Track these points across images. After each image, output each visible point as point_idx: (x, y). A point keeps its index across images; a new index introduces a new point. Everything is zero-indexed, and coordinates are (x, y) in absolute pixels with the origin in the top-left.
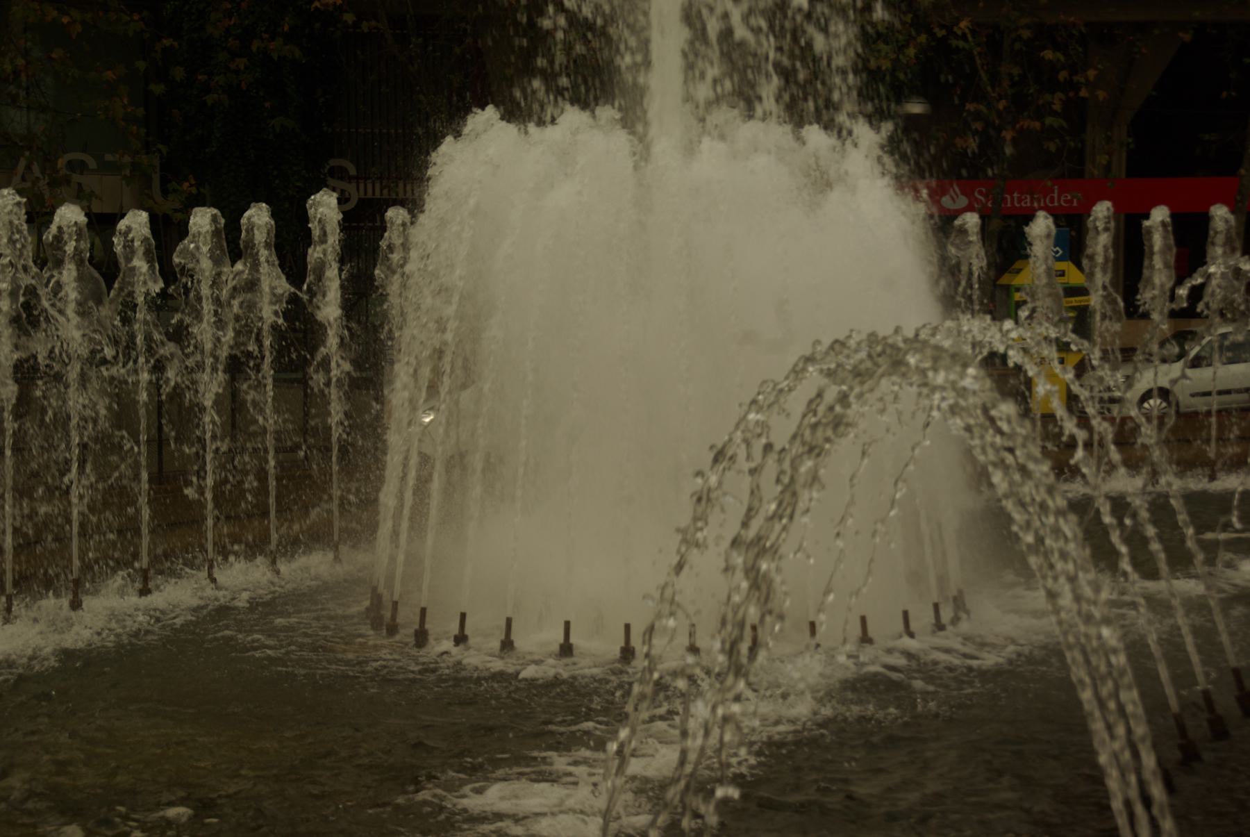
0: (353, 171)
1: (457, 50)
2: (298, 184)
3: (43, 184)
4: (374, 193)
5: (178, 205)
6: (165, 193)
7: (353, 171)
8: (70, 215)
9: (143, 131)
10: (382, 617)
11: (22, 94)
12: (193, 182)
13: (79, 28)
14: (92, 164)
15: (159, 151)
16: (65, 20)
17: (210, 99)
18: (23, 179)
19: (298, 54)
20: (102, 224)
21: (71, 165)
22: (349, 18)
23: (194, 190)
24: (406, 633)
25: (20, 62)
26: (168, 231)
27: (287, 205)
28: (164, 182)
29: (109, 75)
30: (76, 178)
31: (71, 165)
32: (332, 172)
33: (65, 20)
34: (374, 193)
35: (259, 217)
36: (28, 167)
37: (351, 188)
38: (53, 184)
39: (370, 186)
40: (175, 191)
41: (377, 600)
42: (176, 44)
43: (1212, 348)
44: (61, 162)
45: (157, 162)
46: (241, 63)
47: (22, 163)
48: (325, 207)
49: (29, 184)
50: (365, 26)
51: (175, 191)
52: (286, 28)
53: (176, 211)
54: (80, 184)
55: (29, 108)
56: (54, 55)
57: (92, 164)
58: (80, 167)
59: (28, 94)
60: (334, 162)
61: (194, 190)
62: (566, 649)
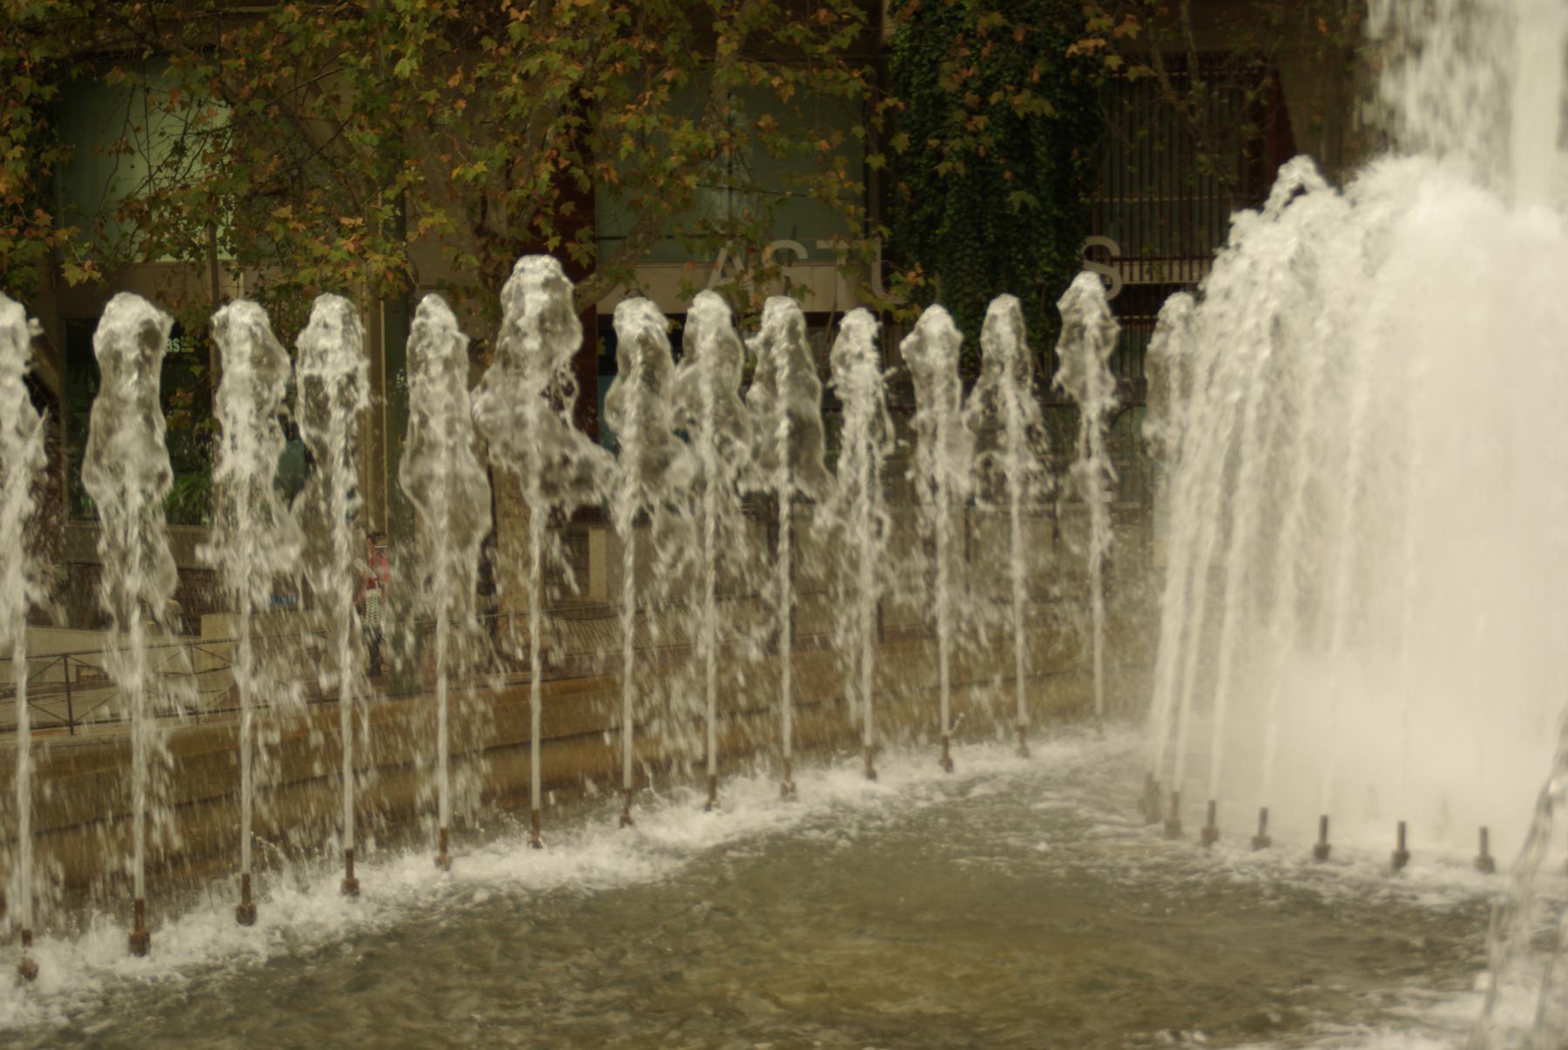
0: (1115, 251)
1: (1250, 95)
2: (1048, 269)
3: (748, 277)
4: (1131, 278)
5: (901, 301)
6: (887, 285)
7: (1115, 251)
8: (779, 312)
9: (862, 210)
10: (1157, 803)
11: (724, 172)
12: (920, 271)
13: (791, 91)
14: (802, 253)
15: (880, 234)
16: (776, 82)
17: (943, 168)
18: (724, 275)
19: (1048, 109)
20: (823, 325)
21: (777, 255)
22: (1113, 61)
23: (921, 281)
24: (1193, 828)
25: (724, 135)
26: (892, 330)
27: (1034, 296)
28: (886, 271)
29: (823, 145)
30: (786, 271)
31: (777, 255)
32: (1090, 254)
33: (776, 82)
34: (1131, 278)
35: (1003, 311)
36: (729, 260)
37: (1113, 272)
38: (760, 278)
39: (1176, 268)
40: (898, 283)
41: (1153, 788)
42: (901, 105)
43: (739, 629)
44: (768, 252)
45: (877, 247)
46: (981, 121)
47: (723, 253)
48: (1087, 294)
49: (731, 280)
50: (1132, 74)
51: (898, 283)
52: (1036, 77)
53: (899, 307)
54: (787, 278)
55: (731, 189)
56: (761, 124)
57: (802, 253)
58: (788, 257)
59: (730, 172)
60: (1093, 241)
61: (921, 281)
62: (1401, 858)
